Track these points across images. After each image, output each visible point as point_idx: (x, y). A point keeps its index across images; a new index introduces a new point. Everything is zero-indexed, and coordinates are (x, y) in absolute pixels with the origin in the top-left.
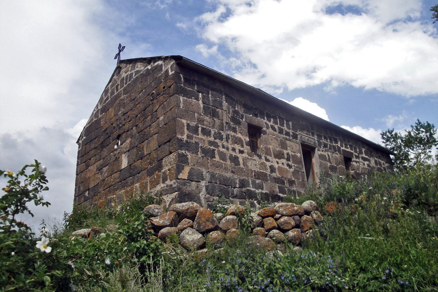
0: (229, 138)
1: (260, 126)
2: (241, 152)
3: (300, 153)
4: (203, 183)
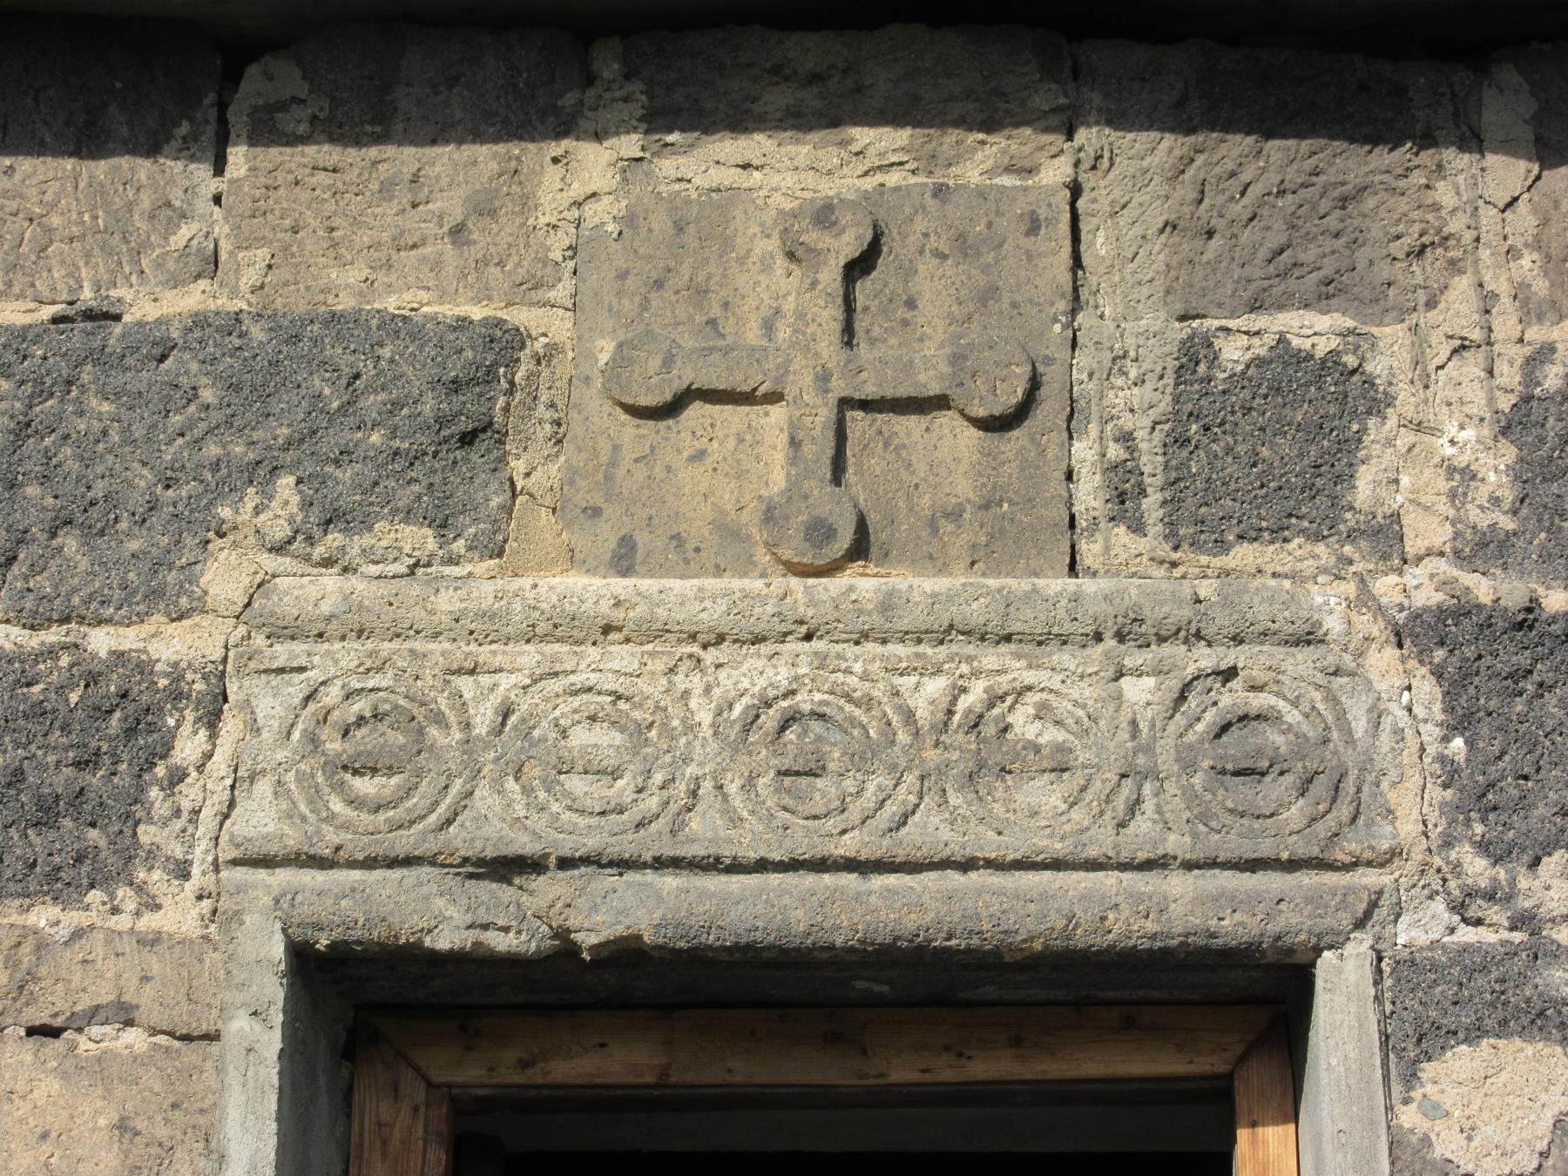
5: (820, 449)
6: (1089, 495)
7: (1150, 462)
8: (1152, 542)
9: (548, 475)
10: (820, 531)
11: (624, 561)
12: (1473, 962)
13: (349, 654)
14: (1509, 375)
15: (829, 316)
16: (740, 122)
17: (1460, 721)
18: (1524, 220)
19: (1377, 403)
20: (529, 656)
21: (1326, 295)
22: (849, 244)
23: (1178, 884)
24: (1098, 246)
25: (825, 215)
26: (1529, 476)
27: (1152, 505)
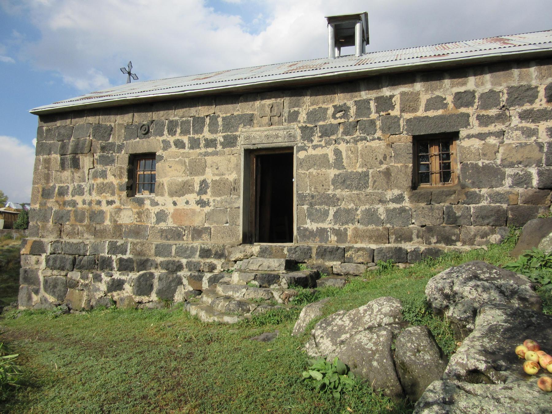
0: (93, 189)
1: (152, 151)
2: (110, 203)
3: (238, 173)
4: (44, 256)
5: (269, 119)
6: (284, 121)
7: (287, 119)
8: (287, 123)
9: (256, 122)
10: (269, 124)
11: (260, 126)
12: (302, 147)
13: (246, 133)
14: (307, 111)
15: (270, 111)
16: (265, 99)
17: (302, 133)
18: (309, 100)
19: (300, 113)
20: (255, 133)
21: (297, 107)
22: (271, 107)
23: (287, 143)
24: (285, 105)
25: (270, 105)
26: (308, 117)
27: (287, 121)
